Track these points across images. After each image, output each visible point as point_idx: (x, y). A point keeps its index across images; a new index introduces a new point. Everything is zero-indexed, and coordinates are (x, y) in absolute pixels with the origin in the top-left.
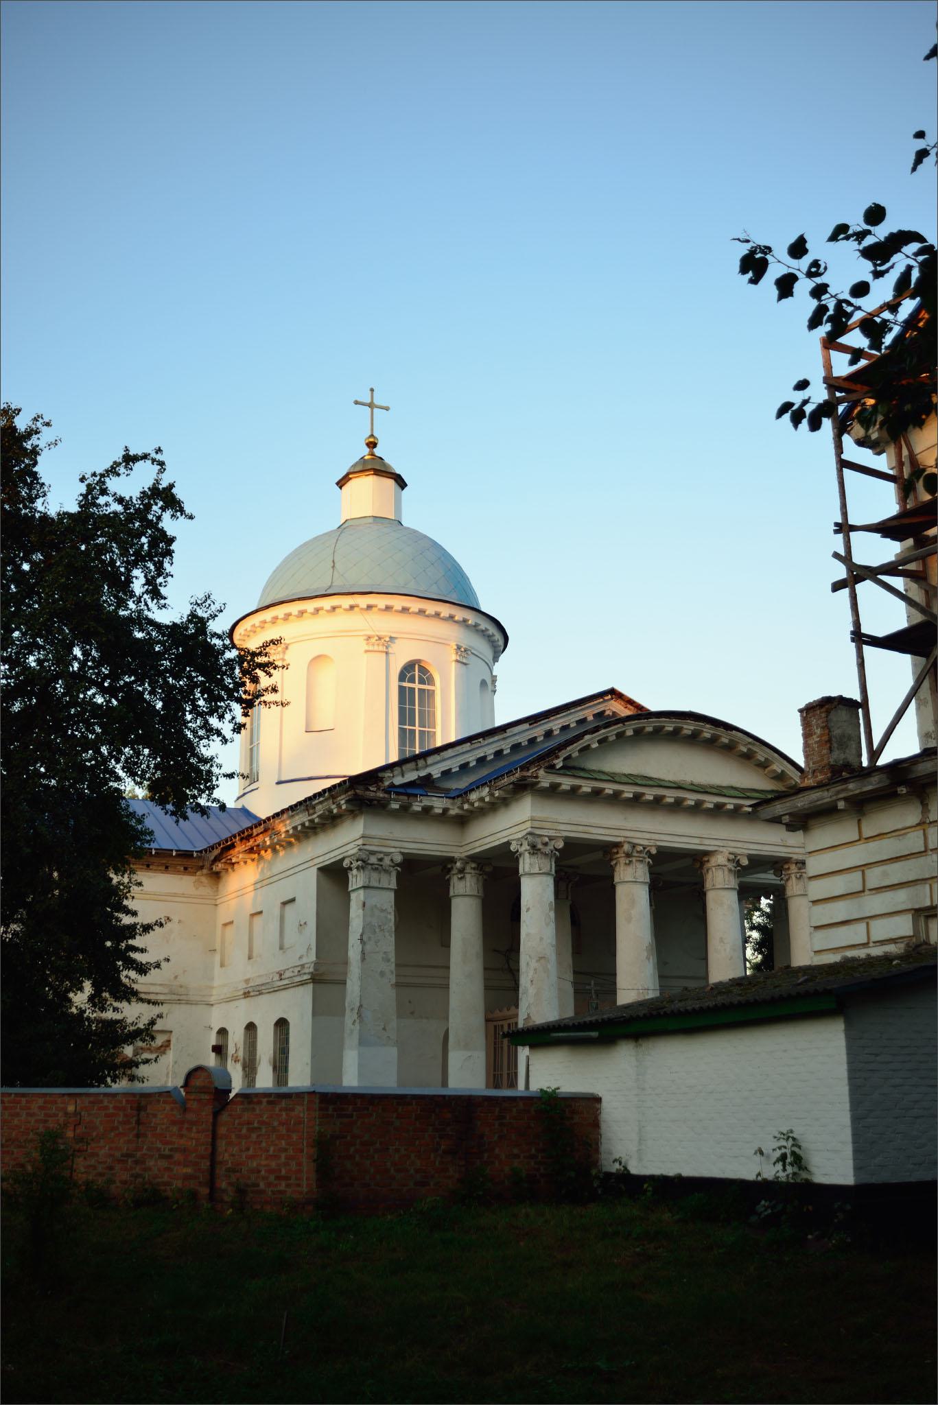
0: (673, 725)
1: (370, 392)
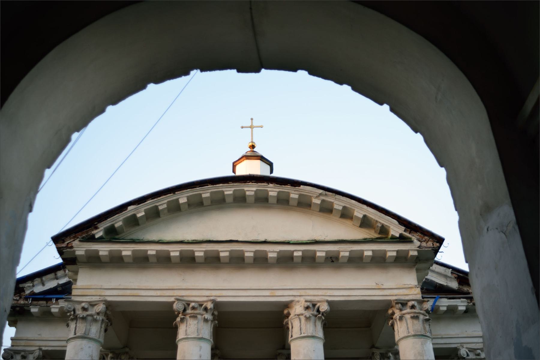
0: (233, 189)
1: (250, 120)
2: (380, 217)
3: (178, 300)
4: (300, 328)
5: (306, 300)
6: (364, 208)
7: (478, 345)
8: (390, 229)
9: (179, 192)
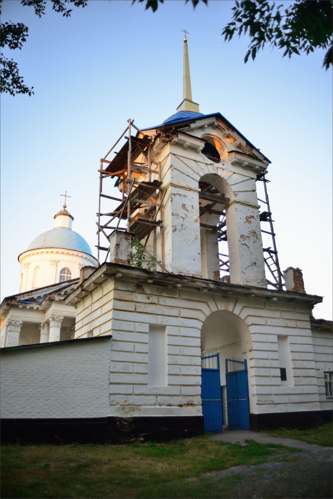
1: (65, 192)
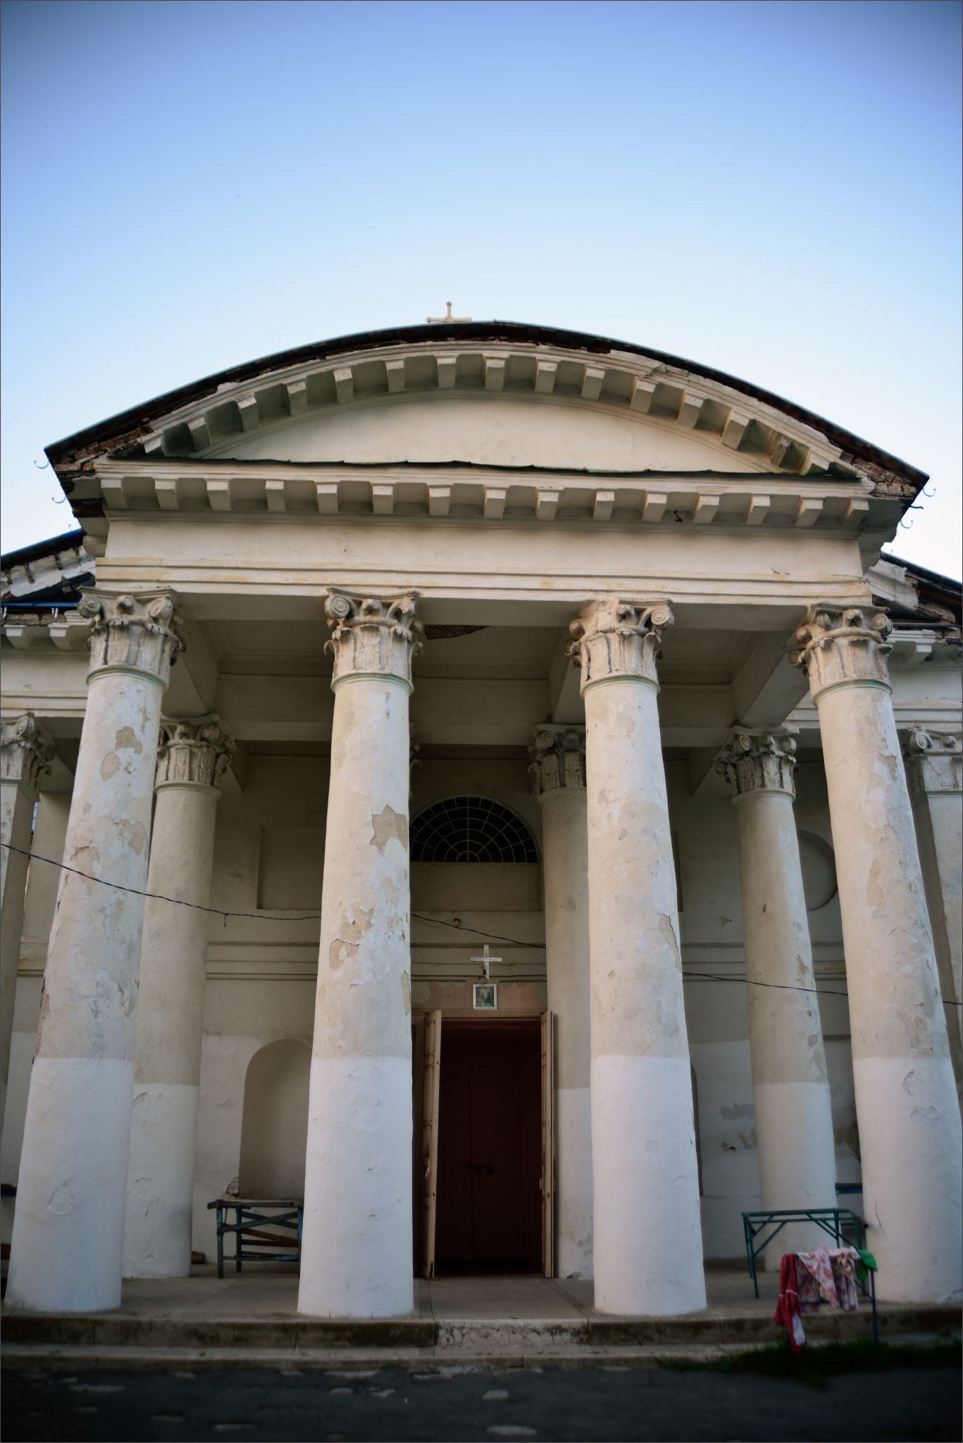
0: (457, 353)
1: (446, 307)
2: (786, 424)
3: (335, 591)
4: (608, 658)
5: (623, 599)
6: (752, 404)
7: (949, 725)
8: (809, 453)
9: (334, 357)
